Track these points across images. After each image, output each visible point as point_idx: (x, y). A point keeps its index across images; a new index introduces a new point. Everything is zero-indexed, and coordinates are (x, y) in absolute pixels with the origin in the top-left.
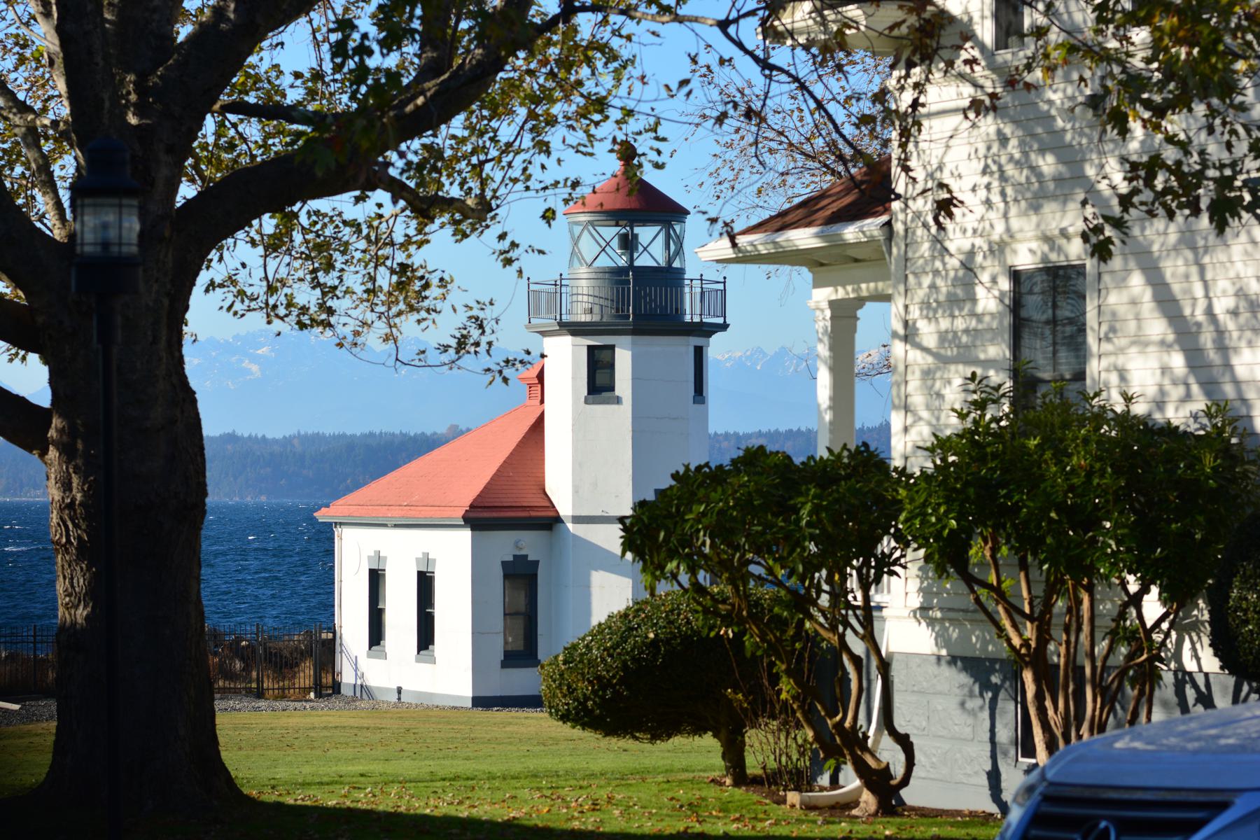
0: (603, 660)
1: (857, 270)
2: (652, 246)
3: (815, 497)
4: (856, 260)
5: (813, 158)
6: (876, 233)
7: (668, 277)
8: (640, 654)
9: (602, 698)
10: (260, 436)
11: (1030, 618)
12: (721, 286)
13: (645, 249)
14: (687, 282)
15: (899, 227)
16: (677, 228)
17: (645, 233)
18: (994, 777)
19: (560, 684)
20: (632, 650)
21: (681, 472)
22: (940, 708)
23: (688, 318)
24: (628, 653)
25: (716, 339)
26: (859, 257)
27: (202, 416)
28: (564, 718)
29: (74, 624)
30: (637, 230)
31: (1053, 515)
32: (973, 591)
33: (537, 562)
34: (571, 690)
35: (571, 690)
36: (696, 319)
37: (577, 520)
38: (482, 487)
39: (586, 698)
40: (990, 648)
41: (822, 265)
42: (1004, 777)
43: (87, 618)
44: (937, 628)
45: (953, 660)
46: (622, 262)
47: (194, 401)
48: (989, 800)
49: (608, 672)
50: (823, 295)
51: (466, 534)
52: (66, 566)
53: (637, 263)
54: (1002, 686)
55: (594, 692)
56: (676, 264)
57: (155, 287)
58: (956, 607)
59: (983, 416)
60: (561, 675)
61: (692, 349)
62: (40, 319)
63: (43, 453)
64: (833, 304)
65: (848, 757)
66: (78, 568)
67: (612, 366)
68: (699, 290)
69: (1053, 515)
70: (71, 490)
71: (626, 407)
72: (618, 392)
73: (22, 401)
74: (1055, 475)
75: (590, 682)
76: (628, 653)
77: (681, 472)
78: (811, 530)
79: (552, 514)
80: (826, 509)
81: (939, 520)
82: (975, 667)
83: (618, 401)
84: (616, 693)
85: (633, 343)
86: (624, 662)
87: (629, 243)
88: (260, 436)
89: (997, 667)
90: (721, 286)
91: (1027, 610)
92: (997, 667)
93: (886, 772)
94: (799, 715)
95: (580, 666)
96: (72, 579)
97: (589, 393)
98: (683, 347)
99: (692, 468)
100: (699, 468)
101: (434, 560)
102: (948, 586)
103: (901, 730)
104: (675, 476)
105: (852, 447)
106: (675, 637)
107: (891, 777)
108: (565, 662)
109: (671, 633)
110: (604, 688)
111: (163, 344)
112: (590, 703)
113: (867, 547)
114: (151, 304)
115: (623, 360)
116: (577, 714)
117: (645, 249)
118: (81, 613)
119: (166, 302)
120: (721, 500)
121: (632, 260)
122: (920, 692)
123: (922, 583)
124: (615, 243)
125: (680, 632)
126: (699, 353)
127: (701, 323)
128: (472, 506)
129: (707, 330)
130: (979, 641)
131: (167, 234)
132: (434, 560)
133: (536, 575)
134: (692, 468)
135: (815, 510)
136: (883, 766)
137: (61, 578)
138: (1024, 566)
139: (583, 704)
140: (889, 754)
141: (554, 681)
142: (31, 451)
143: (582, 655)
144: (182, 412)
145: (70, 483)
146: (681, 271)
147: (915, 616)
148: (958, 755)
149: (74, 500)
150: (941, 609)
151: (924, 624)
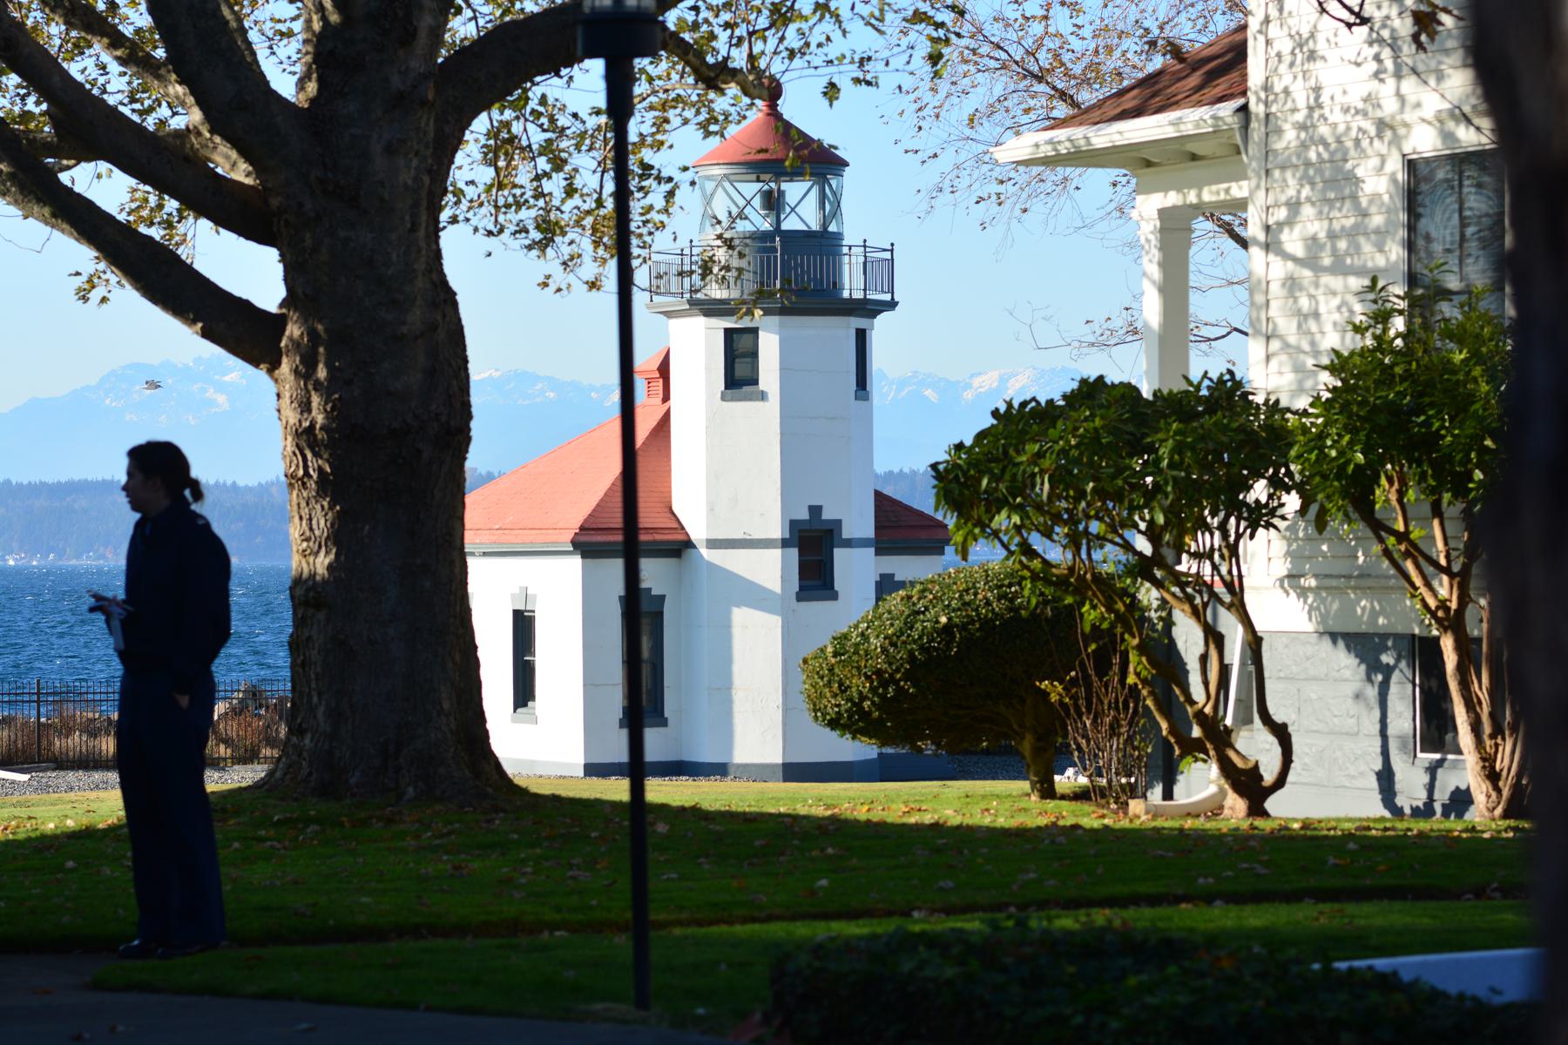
0: (884, 650)
1: (1195, 170)
2: (803, 207)
3: (1176, 433)
4: (1194, 157)
5: (1040, 79)
6: (1229, 120)
7: (822, 245)
8: (929, 641)
9: (883, 697)
10: (229, 483)
11: (1447, 570)
12: (887, 255)
13: (793, 210)
14: (845, 250)
15: (1257, 108)
16: (834, 183)
17: (793, 190)
18: (1386, 779)
19: (829, 682)
20: (920, 637)
21: (1002, 410)
22: (1314, 696)
23: (846, 294)
24: (915, 641)
25: (882, 320)
26: (1200, 152)
27: (464, 322)
28: (834, 724)
29: (313, 576)
30: (784, 186)
31: (1488, 443)
32: (1381, 540)
33: (662, 598)
34: (843, 688)
35: (843, 688)
36: (858, 295)
37: (713, 544)
38: (594, 504)
39: (862, 698)
40: (1381, 621)
41: (1149, 164)
42: (1398, 777)
43: (330, 567)
44: (1310, 601)
45: (1334, 637)
46: (766, 226)
47: (455, 305)
48: (1380, 805)
49: (890, 664)
50: (1150, 206)
51: (576, 561)
52: (303, 504)
53: (785, 226)
54: (1395, 666)
55: (873, 690)
56: (832, 228)
57: (415, 163)
58: (1335, 572)
59: (1385, 330)
60: (831, 670)
61: (853, 333)
62: (275, 202)
63: (273, 367)
64: (1163, 213)
65: (1212, 753)
66: (318, 507)
67: (754, 354)
68: (862, 259)
69: (1488, 443)
70: (309, 411)
71: (773, 404)
72: (762, 385)
73: (245, 305)
74: (1487, 393)
75: (868, 678)
76: (915, 641)
77: (1002, 410)
78: (1175, 473)
79: (681, 537)
80: (1192, 448)
81: (1341, 453)
82: (1364, 645)
83: (763, 396)
84: (899, 690)
85: (781, 326)
86: (911, 653)
87: (773, 202)
88: (229, 483)
89: (1390, 643)
90: (887, 255)
91: (1443, 562)
92: (1390, 643)
93: (1255, 773)
94: (1149, 702)
95: (855, 658)
96: (310, 519)
97: (727, 387)
98: (843, 329)
99: (1016, 404)
100: (1024, 404)
101: (535, 596)
102: (1325, 548)
103: (1278, 716)
104: (995, 413)
105: (1214, 375)
106: (973, 622)
107: (1261, 778)
108: (835, 654)
109: (968, 616)
110: (885, 684)
111: (421, 233)
112: (867, 704)
113: (1229, 498)
114: (410, 182)
115: (769, 346)
116: (850, 717)
117: (793, 210)
118: (322, 562)
119: (426, 180)
120: (1061, 438)
121: (778, 222)
122: (1286, 678)
123: (1289, 545)
124: (757, 202)
125: (978, 615)
126: (861, 336)
127: (865, 301)
128: (582, 528)
129: (870, 309)
130: (1365, 611)
131: (430, 96)
132: (535, 596)
133: (662, 613)
134: (1016, 404)
135: (1179, 448)
136: (1251, 765)
137: (297, 519)
138: (1437, 511)
139: (859, 705)
140: (1257, 747)
141: (822, 678)
142: (257, 366)
143: (857, 645)
144: (444, 316)
145: (309, 403)
146: (838, 236)
147: (1282, 586)
148: (1338, 754)
149: (312, 425)
150: (1316, 576)
151: (1293, 594)
